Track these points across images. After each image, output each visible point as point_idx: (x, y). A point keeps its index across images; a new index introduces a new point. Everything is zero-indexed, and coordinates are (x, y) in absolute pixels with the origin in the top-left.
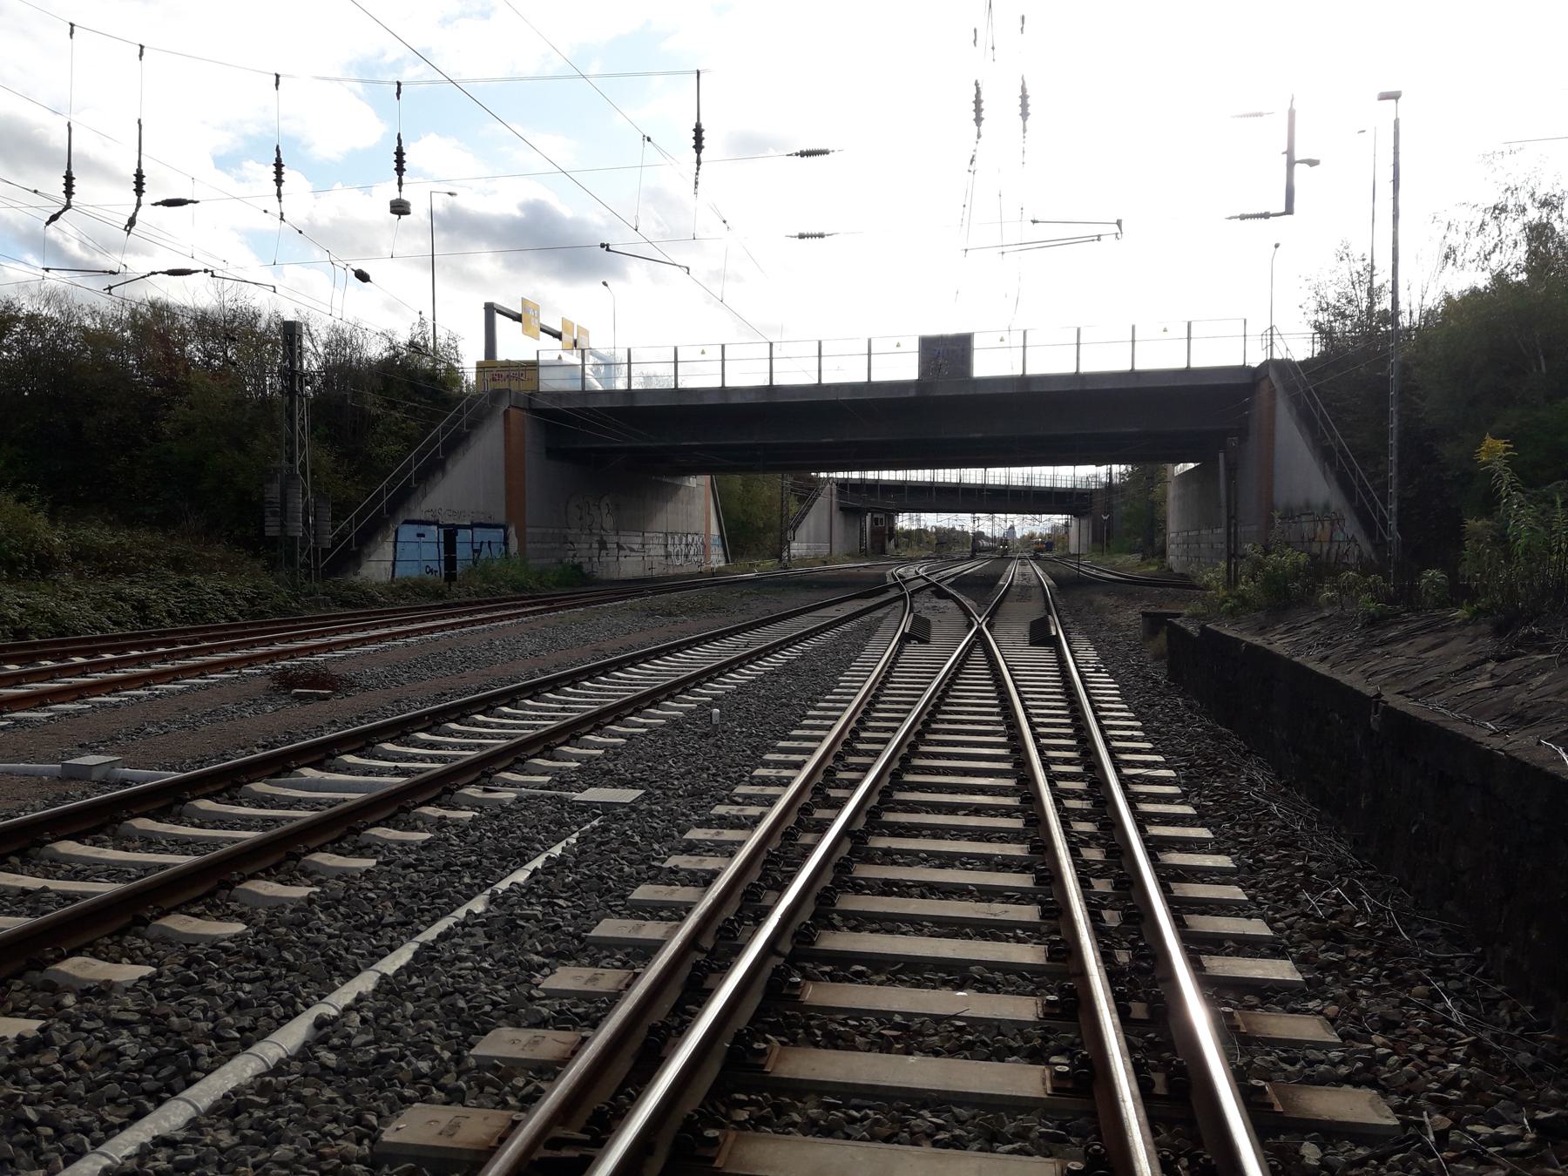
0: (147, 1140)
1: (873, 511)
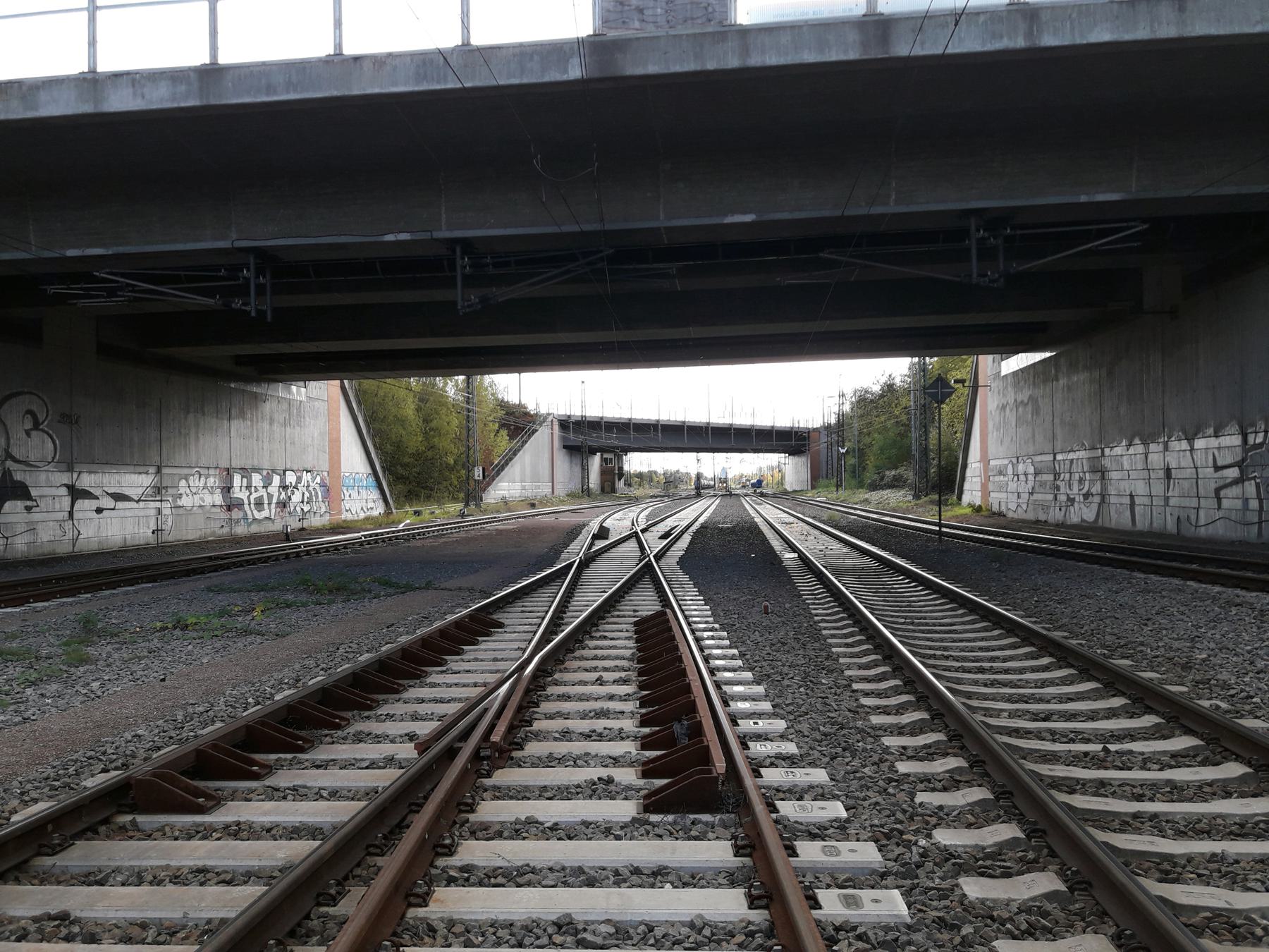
0: (454, 663)
1: (603, 450)
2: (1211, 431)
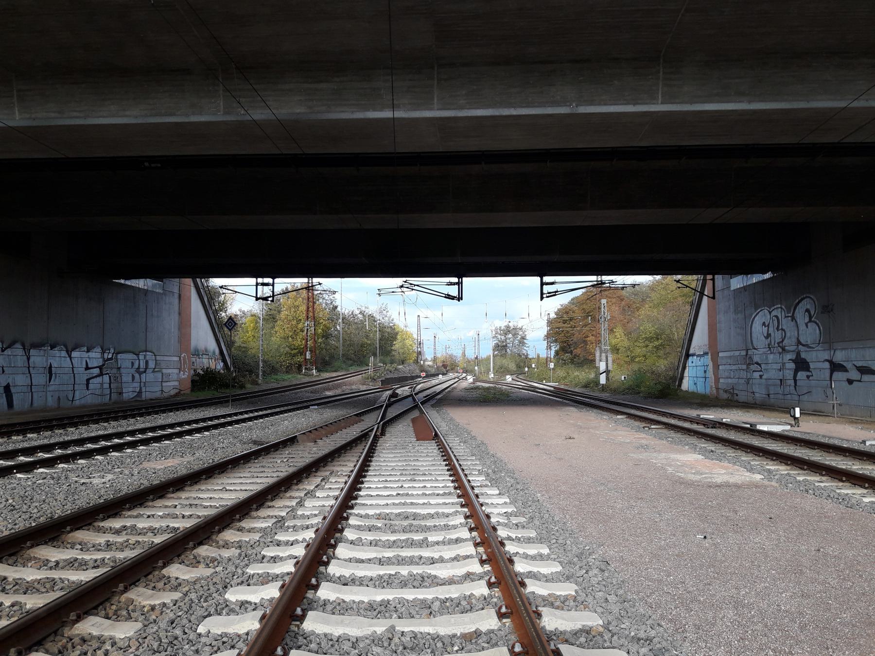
2: (85, 349)
